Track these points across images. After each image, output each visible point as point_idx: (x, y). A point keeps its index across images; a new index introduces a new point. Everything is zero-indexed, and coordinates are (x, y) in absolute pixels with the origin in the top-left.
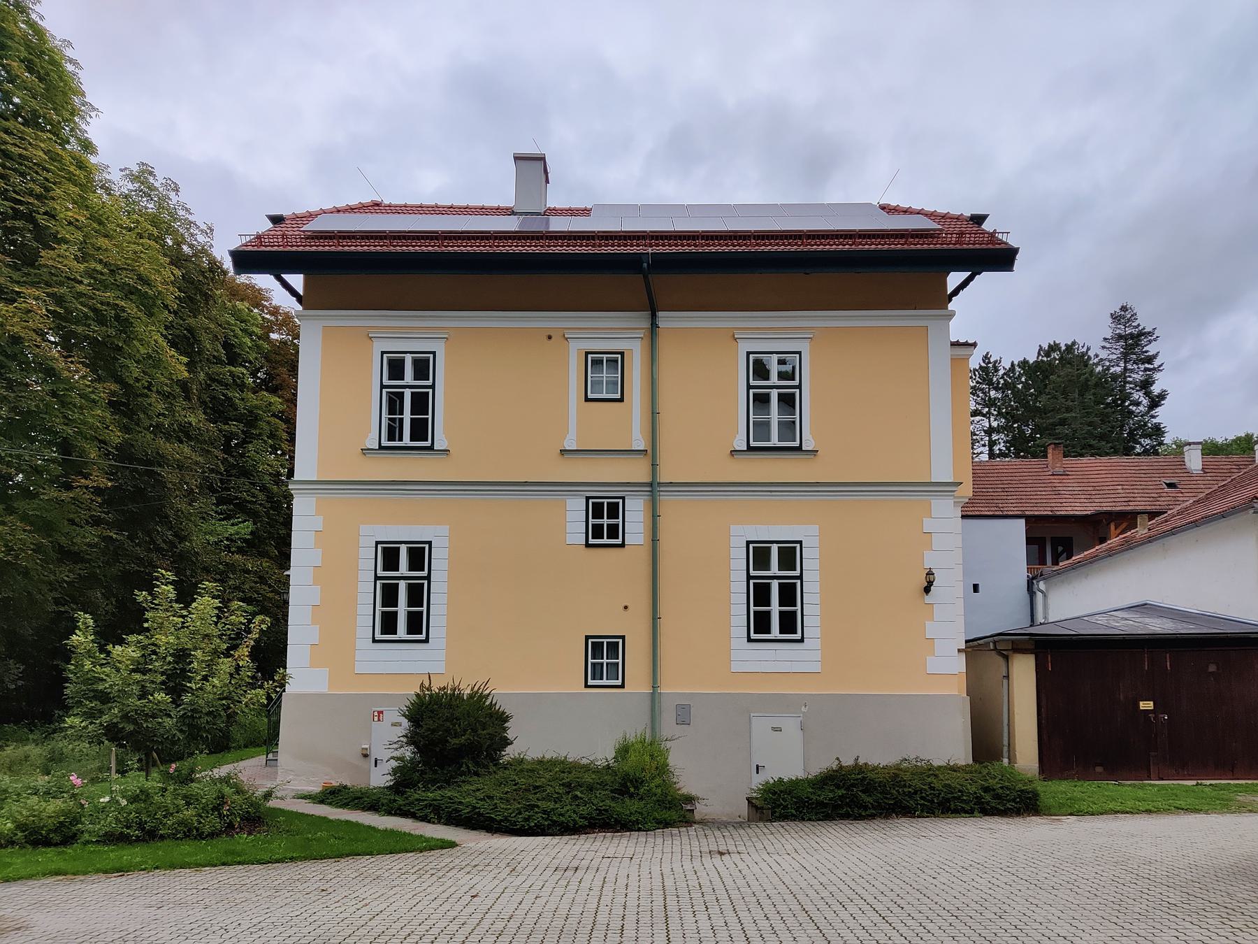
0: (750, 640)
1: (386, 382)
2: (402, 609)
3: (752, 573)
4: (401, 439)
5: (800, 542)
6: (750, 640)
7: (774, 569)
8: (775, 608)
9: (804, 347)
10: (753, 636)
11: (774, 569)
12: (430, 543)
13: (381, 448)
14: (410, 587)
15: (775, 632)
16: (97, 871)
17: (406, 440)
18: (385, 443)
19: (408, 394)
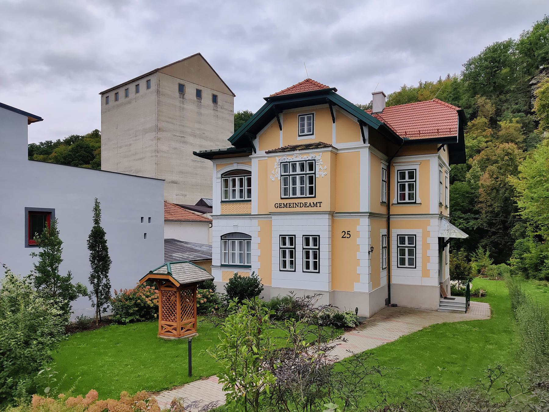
0: (398, 267)
1: (399, 181)
2: (311, 260)
3: (399, 245)
4: (405, 200)
5: (415, 235)
6: (398, 267)
7: (407, 244)
8: (407, 257)
9: (417, 167)
10: (399, 266)
11: (407, 244)
12: (415, 235)
13: (398, 203)
14: (409, 250)
15: (407, 265)
16: (495, 297)
17: (407, 200)
18: (399, 201)
19: (407, 184)
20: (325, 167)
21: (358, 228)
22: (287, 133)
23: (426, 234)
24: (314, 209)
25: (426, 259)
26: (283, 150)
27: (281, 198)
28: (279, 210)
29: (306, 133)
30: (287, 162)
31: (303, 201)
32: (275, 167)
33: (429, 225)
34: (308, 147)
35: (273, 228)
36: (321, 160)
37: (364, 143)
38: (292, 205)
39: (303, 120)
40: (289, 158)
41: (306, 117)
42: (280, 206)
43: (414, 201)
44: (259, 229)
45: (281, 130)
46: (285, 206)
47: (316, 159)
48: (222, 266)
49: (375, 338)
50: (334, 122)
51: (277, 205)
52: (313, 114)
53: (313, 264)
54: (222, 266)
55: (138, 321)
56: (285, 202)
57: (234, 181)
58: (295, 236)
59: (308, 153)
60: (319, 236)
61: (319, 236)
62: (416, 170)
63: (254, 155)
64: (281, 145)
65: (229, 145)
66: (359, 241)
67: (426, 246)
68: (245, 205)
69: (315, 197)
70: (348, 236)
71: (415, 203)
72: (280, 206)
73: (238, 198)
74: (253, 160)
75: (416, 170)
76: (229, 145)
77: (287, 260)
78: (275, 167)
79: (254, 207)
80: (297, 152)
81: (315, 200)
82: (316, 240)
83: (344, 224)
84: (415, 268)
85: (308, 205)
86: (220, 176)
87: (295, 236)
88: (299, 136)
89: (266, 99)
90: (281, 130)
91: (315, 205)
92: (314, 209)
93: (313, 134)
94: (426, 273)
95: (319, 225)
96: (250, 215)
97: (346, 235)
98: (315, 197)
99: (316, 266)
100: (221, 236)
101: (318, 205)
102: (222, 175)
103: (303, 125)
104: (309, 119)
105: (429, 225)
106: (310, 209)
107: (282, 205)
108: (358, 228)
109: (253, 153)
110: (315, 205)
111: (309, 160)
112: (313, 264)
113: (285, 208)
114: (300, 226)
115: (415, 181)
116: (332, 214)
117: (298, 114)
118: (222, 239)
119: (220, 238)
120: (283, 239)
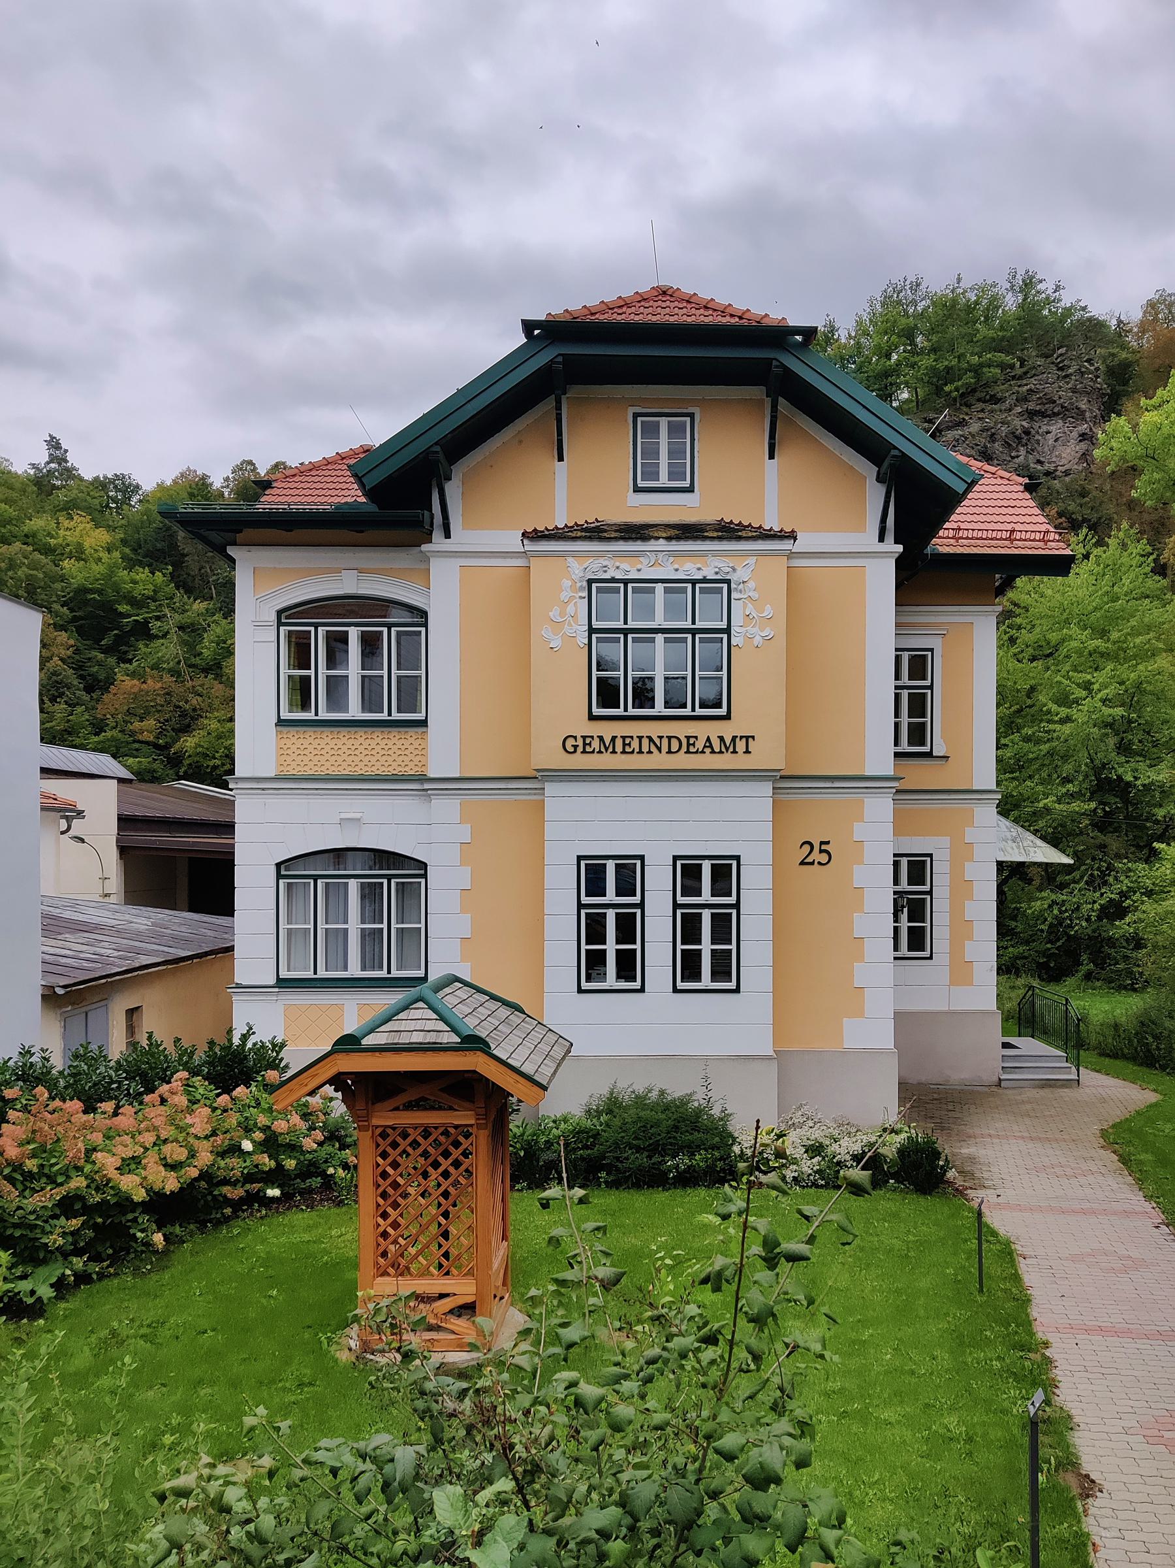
20: (768, 611)
21: (860, 831)
22: (591, 470)
23: (962, 853)
24: (725, 761)
25: (962, 930)
26: (595, 532)
27: (592, 717)
28: (580, 761)
29: (664, 481)
30: (613, 580)
31: (682, 730)
32: (564, 596)
33: (861, 819)
34: (688, 532)
35: (550, 831)
36: (752, 584)
37: (881, 539)
38: (635, 744)
39: (652, 431)
40: (625, 566)
41: (664, 422)
42: (585, 745)
43: (926, 749)
44: (464, 833)
45: (561, 459)
46: (607, 746)
47: (734, 577)
48: (283, 983)
49: (1084, 1212)
50: (771, 457)
51: (570, 742)
52: (692, 416)
53: (706, 956)
54: (283, 983)
55: (83, 1278)
56: (607, 730)
57: (337, 642)
58: (738, 858)
59: (703, 554)
60: (642, 858)
61: (642, 858)
62: (932, 650)
63: (438, 543)
64: (561, 520)
65: (352, 494)
66: (860, 876)
67: (962, 889)
68: (395, 740)
69: (727, 717)
70: (824, 858)
71: (929, 755)
72: (585, 745)
73: (354, 710)
74: (436, 566)
75: (932, 650)
76: (352, 494)
77: (608, 951)
78: (564, 596)
79: (443, 749)
80: (661, 545)
81: (727, 730)
82: (724, 873)
83: (818, 816)
84: (931, 958)
85: (700, 745)
86: (273, 617)
87: (738, 858)
88: (637, 490)
89: (528, 326)
90: (561, 459)
91: (728, 746)
92: (725, 763)
93: (690, 490)
94: (961, 973)
95: (734, 821)
96: (422, 778)
97: (816, 856)
98: (727, 717)
99: (723, 967)
100: (278, 865)
101: (741, 746)
102: (280, 613)
103: (652, 452)
104: (675, 430)
105: (861, 819)
106: (708, 761)
107: (596, 744)
108: (860, 831)
109: (437, 535)
110: (728, 746)
111: (705, 580)
112: (706, 956)
113: (728, 756)
114: (658, 824)
115: (931, 687)
116: (782, 781)
117: (631, 411)
118: (279, 876)
119: (273, 869)
120: (593, 875)
